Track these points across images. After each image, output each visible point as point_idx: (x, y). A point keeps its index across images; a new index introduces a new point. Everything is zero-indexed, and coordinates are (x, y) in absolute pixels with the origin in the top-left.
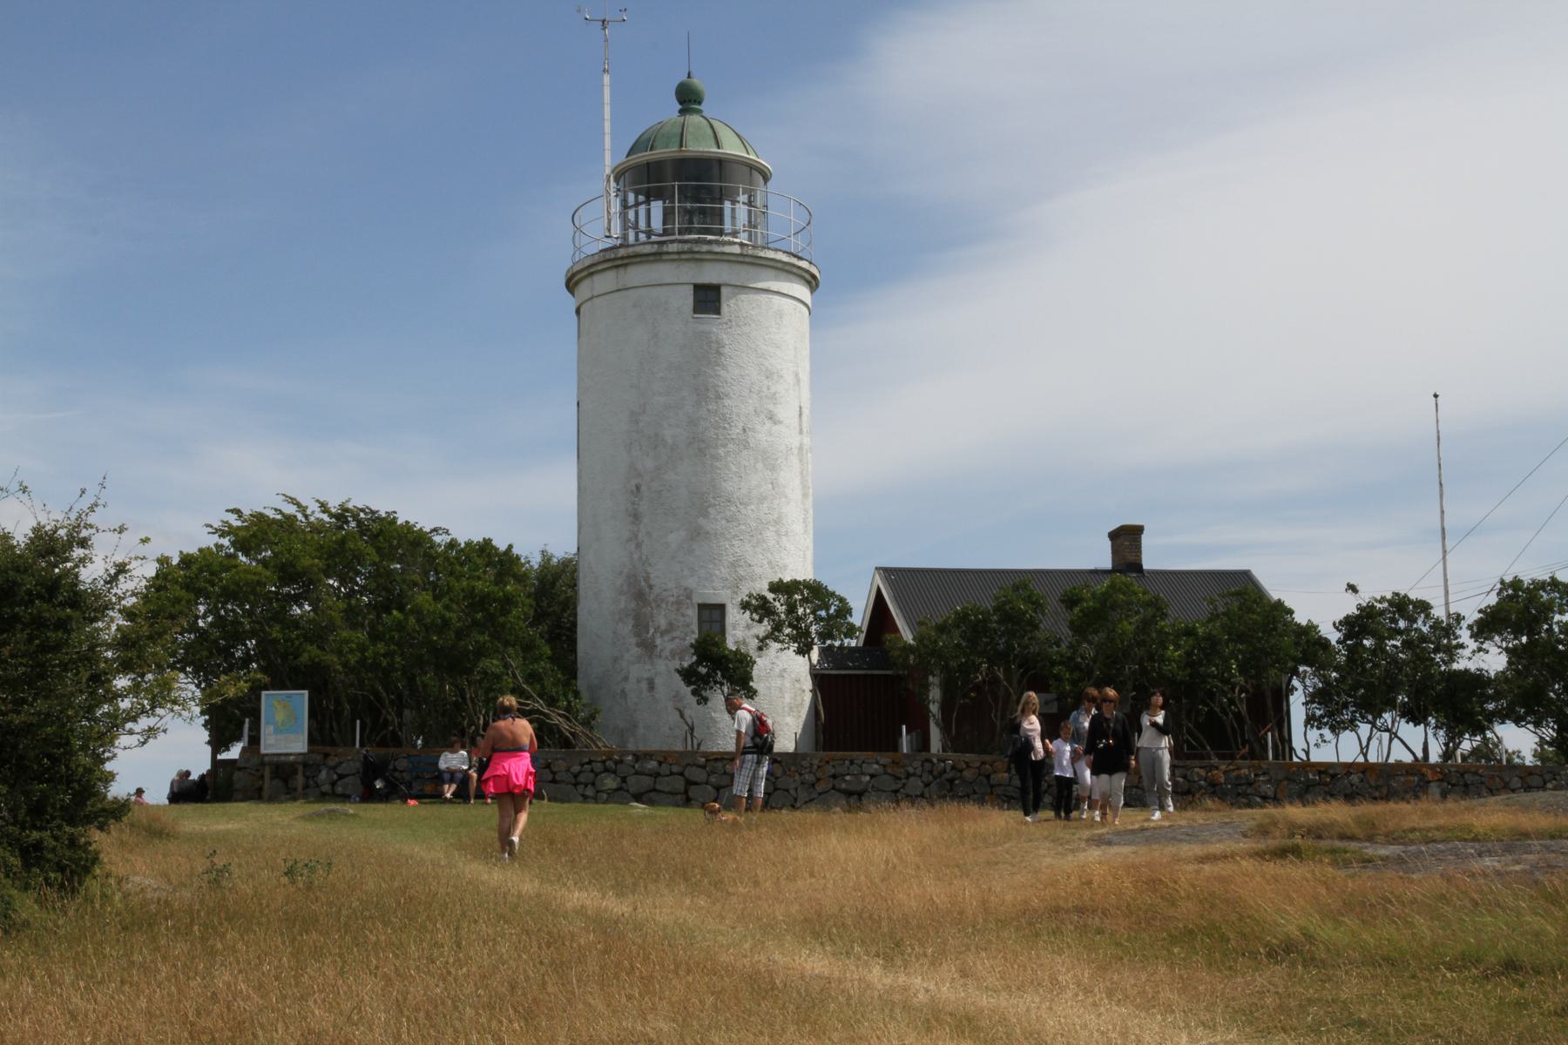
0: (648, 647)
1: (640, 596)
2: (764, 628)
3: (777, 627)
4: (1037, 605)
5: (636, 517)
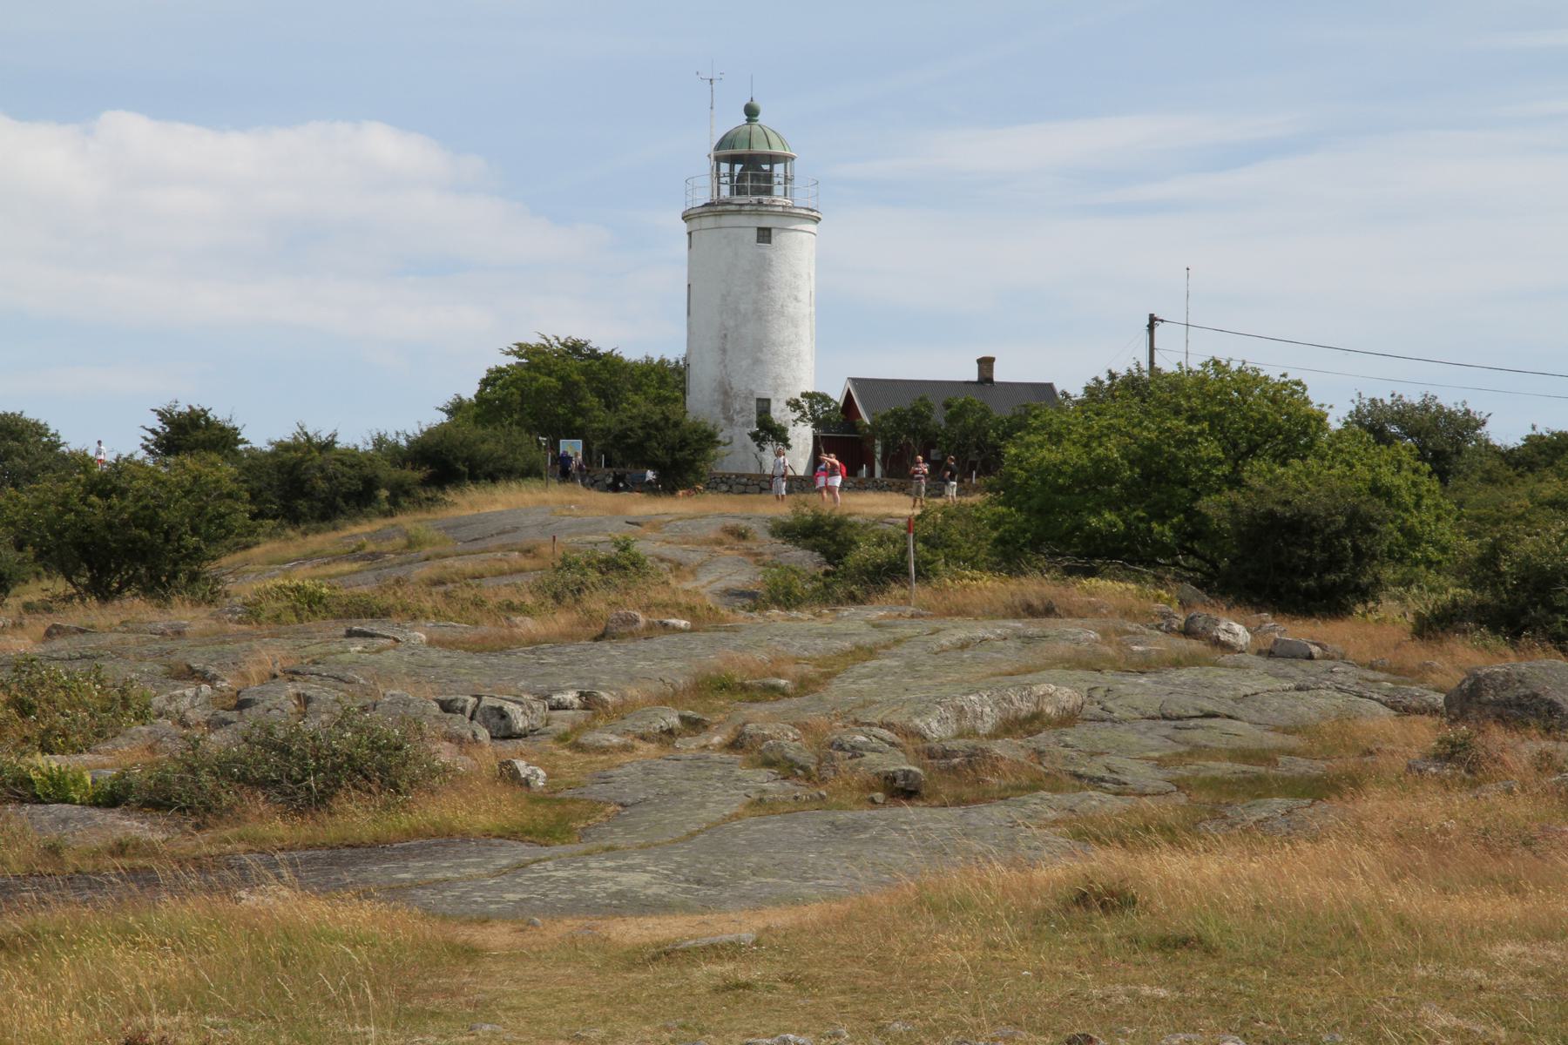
0: (730, 420)
1: (726, 393)
2: (798, 414)
3: (804, 414)
4: (930, 408)
5: (724, 351)
